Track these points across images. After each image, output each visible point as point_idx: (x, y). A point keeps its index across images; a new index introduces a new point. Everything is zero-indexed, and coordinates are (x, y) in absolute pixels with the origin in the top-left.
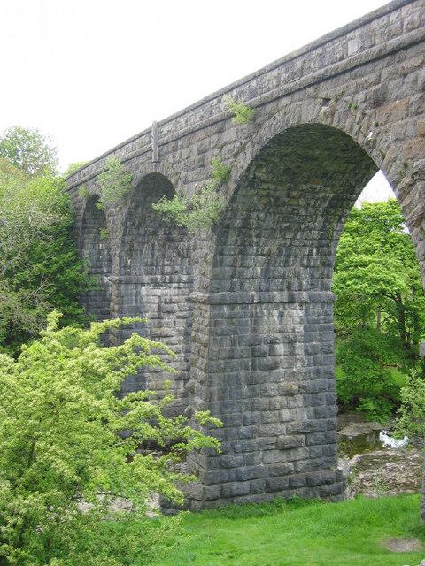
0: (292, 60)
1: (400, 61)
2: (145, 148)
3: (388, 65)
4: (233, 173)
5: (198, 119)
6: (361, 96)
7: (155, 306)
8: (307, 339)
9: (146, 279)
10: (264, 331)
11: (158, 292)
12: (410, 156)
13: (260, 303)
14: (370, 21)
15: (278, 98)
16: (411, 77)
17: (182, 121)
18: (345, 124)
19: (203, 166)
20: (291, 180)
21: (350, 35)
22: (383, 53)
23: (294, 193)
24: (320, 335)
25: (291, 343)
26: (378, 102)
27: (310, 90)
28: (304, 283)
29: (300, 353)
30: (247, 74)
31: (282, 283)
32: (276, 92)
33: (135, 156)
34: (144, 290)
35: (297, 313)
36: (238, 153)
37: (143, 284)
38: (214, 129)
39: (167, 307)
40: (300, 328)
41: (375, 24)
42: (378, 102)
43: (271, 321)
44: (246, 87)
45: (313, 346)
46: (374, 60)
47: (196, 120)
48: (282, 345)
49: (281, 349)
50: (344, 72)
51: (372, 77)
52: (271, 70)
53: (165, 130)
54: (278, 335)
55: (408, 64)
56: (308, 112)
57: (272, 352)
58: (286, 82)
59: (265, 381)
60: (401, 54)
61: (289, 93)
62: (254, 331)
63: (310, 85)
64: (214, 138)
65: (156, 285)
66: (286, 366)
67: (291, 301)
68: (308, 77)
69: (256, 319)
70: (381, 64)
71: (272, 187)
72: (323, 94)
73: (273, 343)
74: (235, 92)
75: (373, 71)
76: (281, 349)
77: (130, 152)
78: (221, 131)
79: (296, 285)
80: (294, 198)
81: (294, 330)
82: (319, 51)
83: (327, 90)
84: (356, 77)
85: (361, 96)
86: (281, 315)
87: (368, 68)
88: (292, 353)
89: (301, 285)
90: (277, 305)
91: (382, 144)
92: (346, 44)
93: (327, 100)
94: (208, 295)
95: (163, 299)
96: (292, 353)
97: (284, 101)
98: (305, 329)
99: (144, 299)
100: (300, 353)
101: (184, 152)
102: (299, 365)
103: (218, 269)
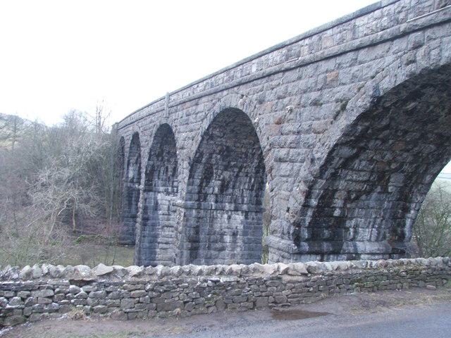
0: (229, 69)
1: (271, 81)
2: (162, 108)
3: (267, 81)
4: (142, 138)
5: (188, 95)
6: (255, 96)
7: (166, 207)
8: (245, 233)
9: (161, 189)
10: (217, 227)
11: (169, 198)
12: (271, 134)
13: (216, 209)
14: (374, 11)
15: (222, 91)
16: (275, 90)
17: (180, 94)
18: (247, 111)
19: (187, 124)
20: (236, 137)
21: (253, 61)
22: (265, 75)
23: (238, 145)
24: (253, 232)
25: (234, 234)
26: (261, 102)
27: (235, 88)
28: (245, 199)
29: (240, 243)
30: (354, 11)
31: (231, 199)
32: (222, 87)
33: (157, 112)
34: (159, 196)
35: (239, 217)
36: (204, 119)
37: (159, 192)
38: (194, 102)
39: (173, 208)
40: (241, 227)
41: (263, 58)
42: (261, 102)
43: (222, 222)
44: (209, 81)
45: (248, 238)
46: (262, 78)
47: (187, 95)
48: (228, 237)
49: (228, 238)
50: (250, 82)
51: (260, 87)
52: (221, 73)
53: (172, 98)
54: (226, 230)
55: (274, 83)
56: (234, 101)
57: (222, 240)
58: (226, 81)
59: (217, 258)
60: (272, 77)
61: (227, 89)
62: (212, 226)
63: (236, 86)
64: (194, 108)
65: (168, 193)
66: (230, 249)
67: (236, 210)
68: (235, 81)
69: (213, 219)
70: (264, 80)
71: (224, 140)
72: (241, 92)
73: (222, 234)
74: (205, 82)
75: (260, 84)
76: (228, 238)
77: (212, 87)
78: (197, 104)
79: (240, 201)
80: (238, 147)
81: (237, 227)
82: (241, 67)
83: (243, 90)
84: (254, 85)
85: (255, 96)
86: (229, 218)
87: (259, 81)
88: (234, 242)
89: (243, 200)
90: (227, 211)
91: (261, 126)
92: (251, 66)
93: (243, 96)
94: (183, 202)
95: (172, 202)
96: (234, 242)
97: (225, 93)
98: (244, 227)
99: (159, 202)
100: (240, 243)
101: (180, 113)
102: (239, 249)
103: (190, 187)
